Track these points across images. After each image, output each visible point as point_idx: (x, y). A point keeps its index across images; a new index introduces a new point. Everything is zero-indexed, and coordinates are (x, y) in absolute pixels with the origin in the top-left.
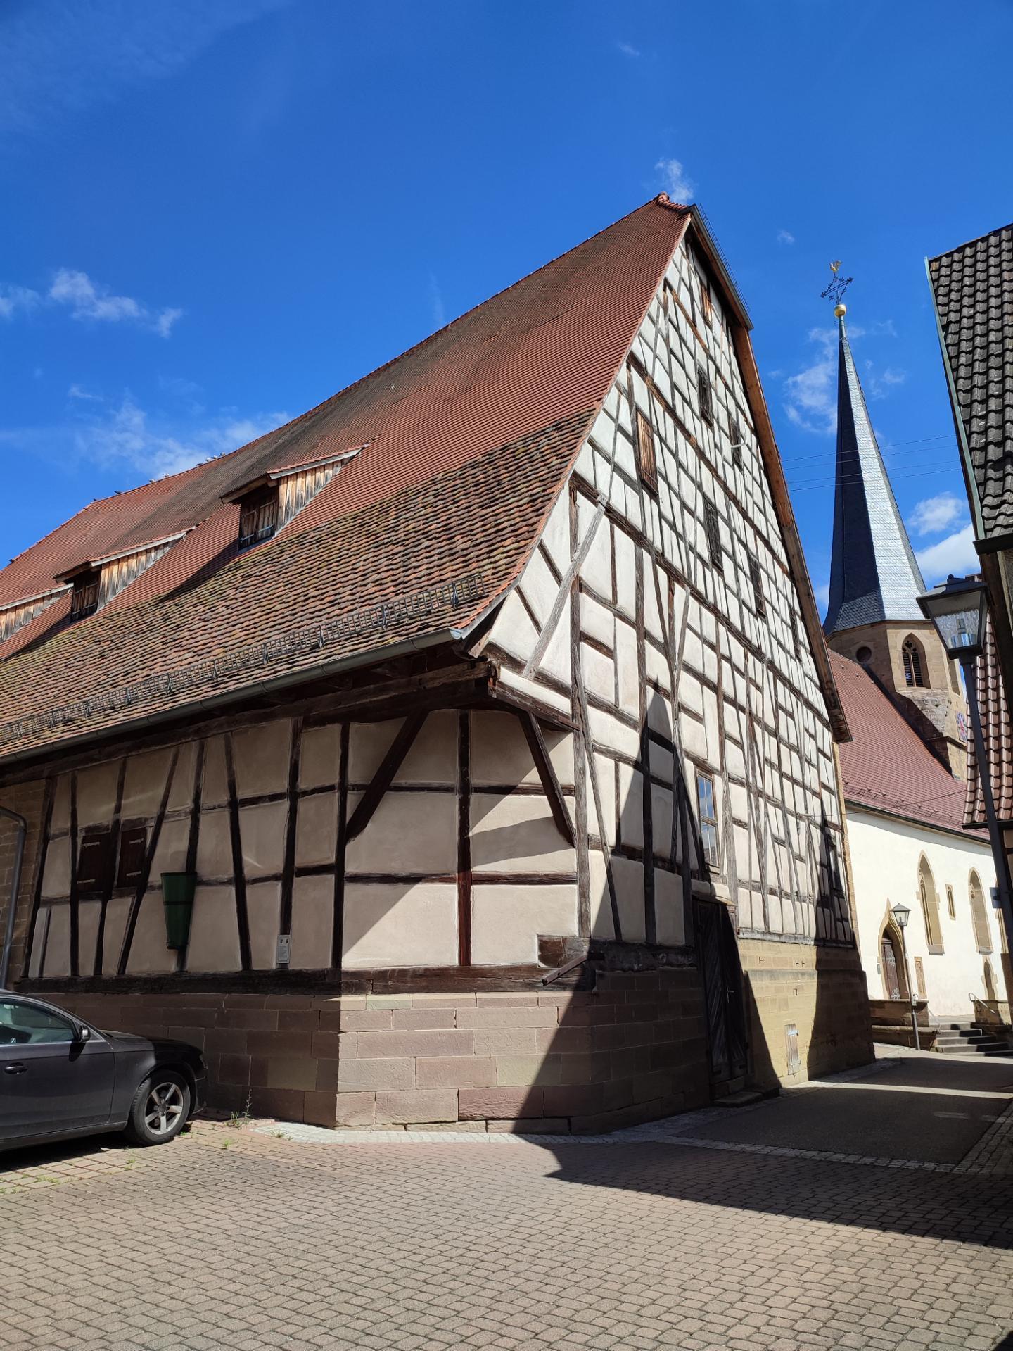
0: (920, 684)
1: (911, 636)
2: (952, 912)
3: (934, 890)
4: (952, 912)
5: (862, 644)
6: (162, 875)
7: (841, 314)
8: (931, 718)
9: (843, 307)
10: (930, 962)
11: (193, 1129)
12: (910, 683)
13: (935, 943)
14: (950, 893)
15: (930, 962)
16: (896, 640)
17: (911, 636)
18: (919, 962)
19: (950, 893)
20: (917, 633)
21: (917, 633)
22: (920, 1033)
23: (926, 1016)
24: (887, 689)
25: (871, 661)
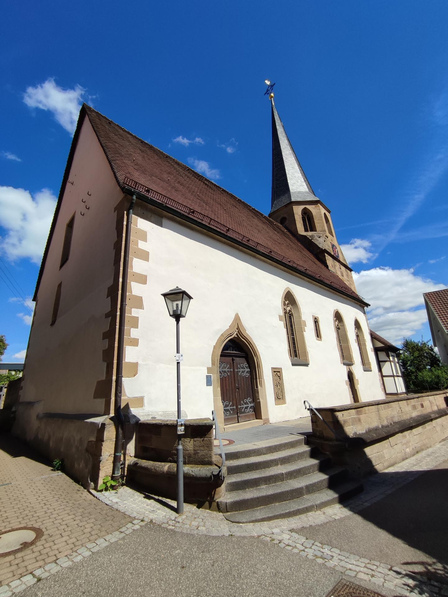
0: (312, 230)
1: (305, 208)
2: (318, 335)
3: (300, 317)
4: (318, 335)
5: (282, 216)
6: (95, 397)
7: (272, 97)
8: (316, 243)
9: (272, 95)
10: (291, 374)
11: (353, 432)
12: (306, 230)
13: (297, 354)
14: (316, 322)
15: (291, 374)
16: (298, 211)
17: (305, 208)
18: (277, 373)
19: (316, 322)
20: (309, 207)
21: (309, 207)
22: (187, 477)
23: (209, 446)
24: (294, 233)
25: (287, 223)
